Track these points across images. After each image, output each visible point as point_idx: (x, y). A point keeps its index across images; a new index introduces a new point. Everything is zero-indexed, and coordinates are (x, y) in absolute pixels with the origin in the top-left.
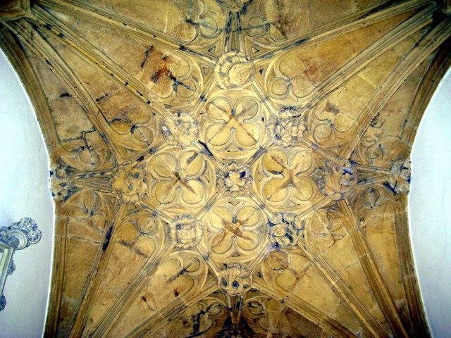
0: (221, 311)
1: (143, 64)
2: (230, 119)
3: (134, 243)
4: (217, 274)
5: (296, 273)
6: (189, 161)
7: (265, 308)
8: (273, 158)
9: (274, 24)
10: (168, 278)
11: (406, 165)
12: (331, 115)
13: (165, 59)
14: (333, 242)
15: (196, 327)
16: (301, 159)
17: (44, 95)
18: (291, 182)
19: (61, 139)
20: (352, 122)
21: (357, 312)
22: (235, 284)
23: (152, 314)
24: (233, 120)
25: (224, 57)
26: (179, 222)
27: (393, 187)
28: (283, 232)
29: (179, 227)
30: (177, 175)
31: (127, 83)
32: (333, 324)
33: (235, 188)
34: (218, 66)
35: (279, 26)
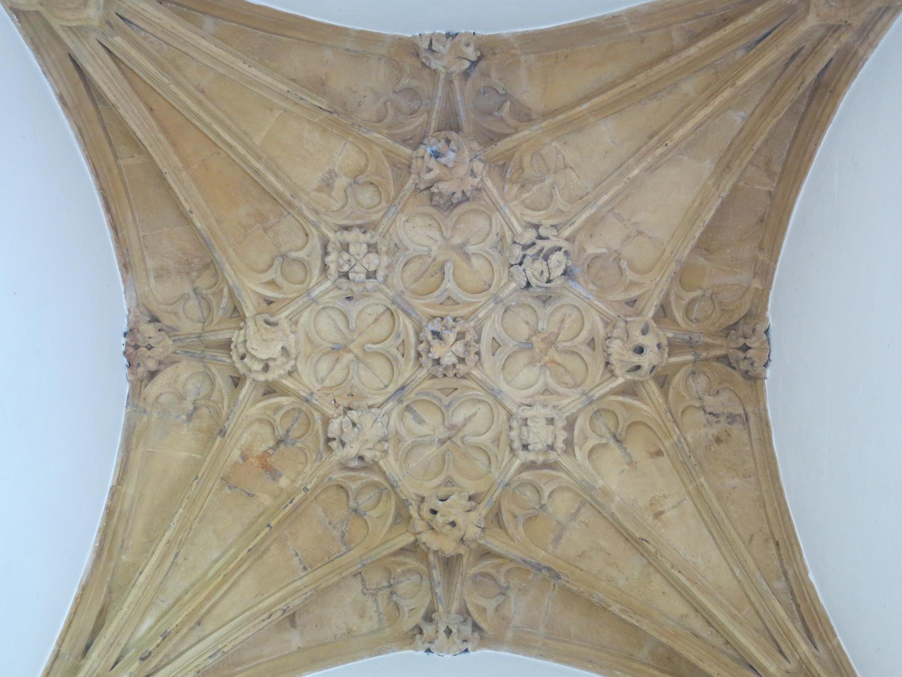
0: (705, 373)
1: (249, 494)
2: (351, 351)
3: (559, 522)
4: (620, 381)
5: (628, 237)
6: (421, 421)
7: (698, 293)
8: (417, 280)
9: (193, 282)
10: (626, 467)
11: (425, 45)
12: (341, 182)
13: (244, 457)
14: (568, 170)
15: (732, 418)
16: (418, 233)
17: (291, 654)
18: (461, 249)
19: (376, 626)
20: (348, 146)
21: (689, 125)
22: (640, 350)
23: (688, 504)
24: (352, 347)
25: (239, 365)
26: (517, 445)
27: (467, 64)
28: (539, 265)
29: (525, 447)
30: (442, 442)
31: (269, 526)
32: (724, 167)
33: (459, 347)
34: (253, 375)
35: (195, 274)
